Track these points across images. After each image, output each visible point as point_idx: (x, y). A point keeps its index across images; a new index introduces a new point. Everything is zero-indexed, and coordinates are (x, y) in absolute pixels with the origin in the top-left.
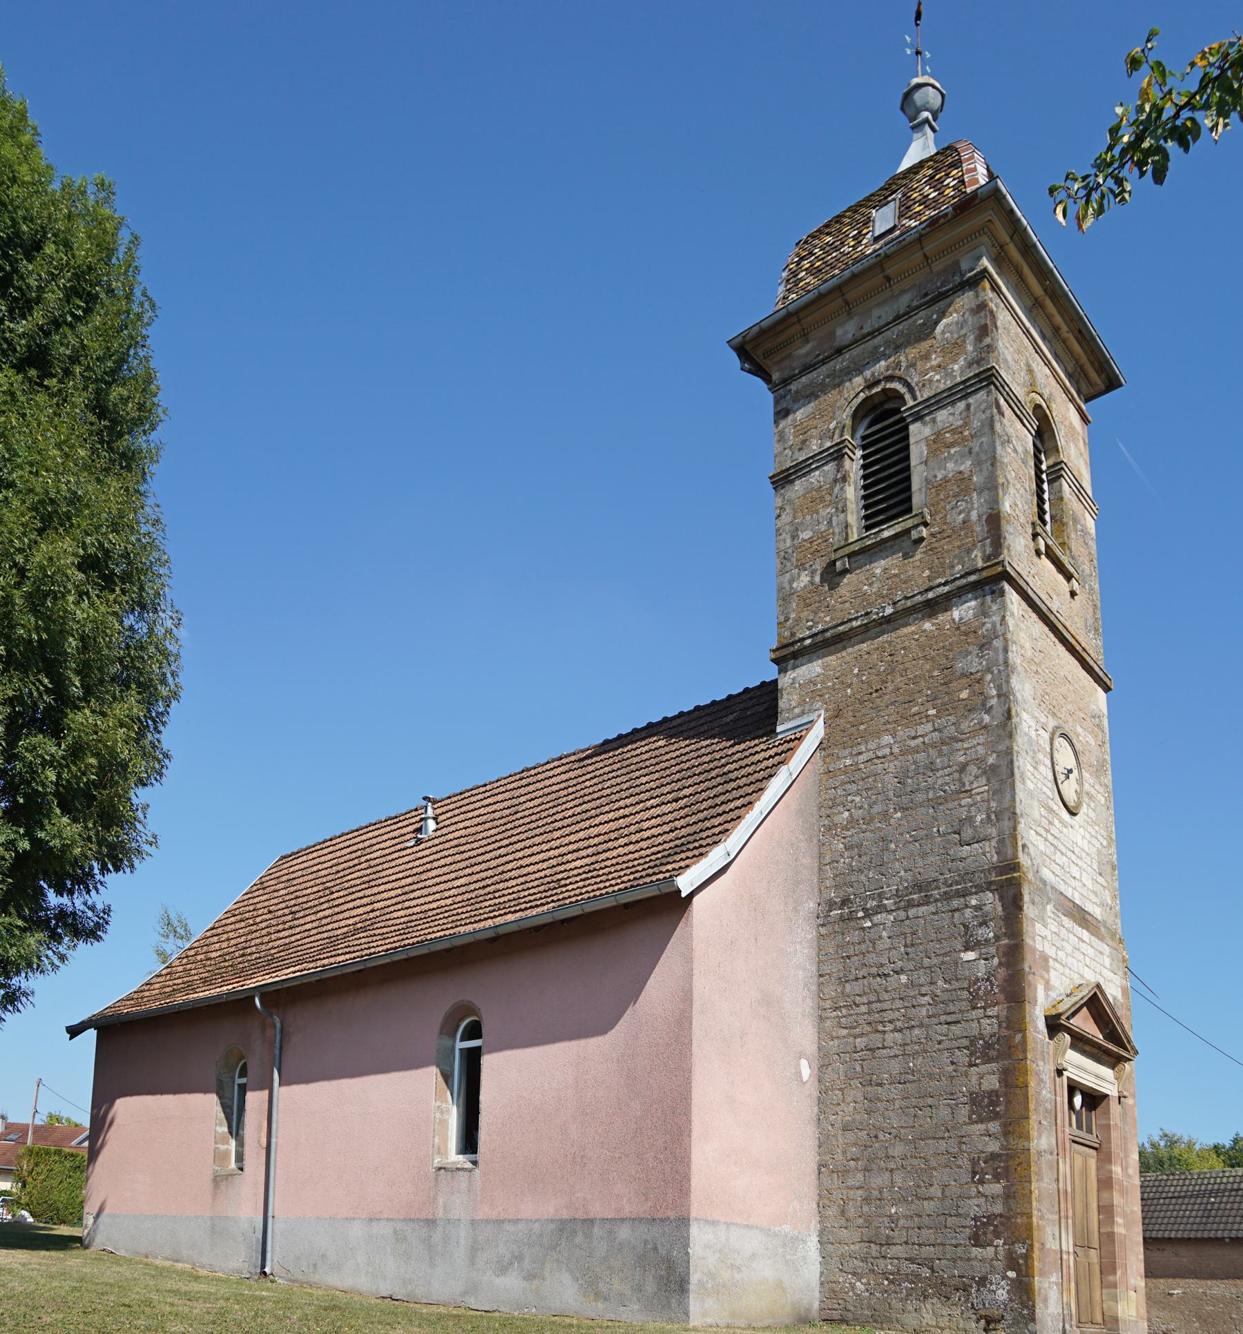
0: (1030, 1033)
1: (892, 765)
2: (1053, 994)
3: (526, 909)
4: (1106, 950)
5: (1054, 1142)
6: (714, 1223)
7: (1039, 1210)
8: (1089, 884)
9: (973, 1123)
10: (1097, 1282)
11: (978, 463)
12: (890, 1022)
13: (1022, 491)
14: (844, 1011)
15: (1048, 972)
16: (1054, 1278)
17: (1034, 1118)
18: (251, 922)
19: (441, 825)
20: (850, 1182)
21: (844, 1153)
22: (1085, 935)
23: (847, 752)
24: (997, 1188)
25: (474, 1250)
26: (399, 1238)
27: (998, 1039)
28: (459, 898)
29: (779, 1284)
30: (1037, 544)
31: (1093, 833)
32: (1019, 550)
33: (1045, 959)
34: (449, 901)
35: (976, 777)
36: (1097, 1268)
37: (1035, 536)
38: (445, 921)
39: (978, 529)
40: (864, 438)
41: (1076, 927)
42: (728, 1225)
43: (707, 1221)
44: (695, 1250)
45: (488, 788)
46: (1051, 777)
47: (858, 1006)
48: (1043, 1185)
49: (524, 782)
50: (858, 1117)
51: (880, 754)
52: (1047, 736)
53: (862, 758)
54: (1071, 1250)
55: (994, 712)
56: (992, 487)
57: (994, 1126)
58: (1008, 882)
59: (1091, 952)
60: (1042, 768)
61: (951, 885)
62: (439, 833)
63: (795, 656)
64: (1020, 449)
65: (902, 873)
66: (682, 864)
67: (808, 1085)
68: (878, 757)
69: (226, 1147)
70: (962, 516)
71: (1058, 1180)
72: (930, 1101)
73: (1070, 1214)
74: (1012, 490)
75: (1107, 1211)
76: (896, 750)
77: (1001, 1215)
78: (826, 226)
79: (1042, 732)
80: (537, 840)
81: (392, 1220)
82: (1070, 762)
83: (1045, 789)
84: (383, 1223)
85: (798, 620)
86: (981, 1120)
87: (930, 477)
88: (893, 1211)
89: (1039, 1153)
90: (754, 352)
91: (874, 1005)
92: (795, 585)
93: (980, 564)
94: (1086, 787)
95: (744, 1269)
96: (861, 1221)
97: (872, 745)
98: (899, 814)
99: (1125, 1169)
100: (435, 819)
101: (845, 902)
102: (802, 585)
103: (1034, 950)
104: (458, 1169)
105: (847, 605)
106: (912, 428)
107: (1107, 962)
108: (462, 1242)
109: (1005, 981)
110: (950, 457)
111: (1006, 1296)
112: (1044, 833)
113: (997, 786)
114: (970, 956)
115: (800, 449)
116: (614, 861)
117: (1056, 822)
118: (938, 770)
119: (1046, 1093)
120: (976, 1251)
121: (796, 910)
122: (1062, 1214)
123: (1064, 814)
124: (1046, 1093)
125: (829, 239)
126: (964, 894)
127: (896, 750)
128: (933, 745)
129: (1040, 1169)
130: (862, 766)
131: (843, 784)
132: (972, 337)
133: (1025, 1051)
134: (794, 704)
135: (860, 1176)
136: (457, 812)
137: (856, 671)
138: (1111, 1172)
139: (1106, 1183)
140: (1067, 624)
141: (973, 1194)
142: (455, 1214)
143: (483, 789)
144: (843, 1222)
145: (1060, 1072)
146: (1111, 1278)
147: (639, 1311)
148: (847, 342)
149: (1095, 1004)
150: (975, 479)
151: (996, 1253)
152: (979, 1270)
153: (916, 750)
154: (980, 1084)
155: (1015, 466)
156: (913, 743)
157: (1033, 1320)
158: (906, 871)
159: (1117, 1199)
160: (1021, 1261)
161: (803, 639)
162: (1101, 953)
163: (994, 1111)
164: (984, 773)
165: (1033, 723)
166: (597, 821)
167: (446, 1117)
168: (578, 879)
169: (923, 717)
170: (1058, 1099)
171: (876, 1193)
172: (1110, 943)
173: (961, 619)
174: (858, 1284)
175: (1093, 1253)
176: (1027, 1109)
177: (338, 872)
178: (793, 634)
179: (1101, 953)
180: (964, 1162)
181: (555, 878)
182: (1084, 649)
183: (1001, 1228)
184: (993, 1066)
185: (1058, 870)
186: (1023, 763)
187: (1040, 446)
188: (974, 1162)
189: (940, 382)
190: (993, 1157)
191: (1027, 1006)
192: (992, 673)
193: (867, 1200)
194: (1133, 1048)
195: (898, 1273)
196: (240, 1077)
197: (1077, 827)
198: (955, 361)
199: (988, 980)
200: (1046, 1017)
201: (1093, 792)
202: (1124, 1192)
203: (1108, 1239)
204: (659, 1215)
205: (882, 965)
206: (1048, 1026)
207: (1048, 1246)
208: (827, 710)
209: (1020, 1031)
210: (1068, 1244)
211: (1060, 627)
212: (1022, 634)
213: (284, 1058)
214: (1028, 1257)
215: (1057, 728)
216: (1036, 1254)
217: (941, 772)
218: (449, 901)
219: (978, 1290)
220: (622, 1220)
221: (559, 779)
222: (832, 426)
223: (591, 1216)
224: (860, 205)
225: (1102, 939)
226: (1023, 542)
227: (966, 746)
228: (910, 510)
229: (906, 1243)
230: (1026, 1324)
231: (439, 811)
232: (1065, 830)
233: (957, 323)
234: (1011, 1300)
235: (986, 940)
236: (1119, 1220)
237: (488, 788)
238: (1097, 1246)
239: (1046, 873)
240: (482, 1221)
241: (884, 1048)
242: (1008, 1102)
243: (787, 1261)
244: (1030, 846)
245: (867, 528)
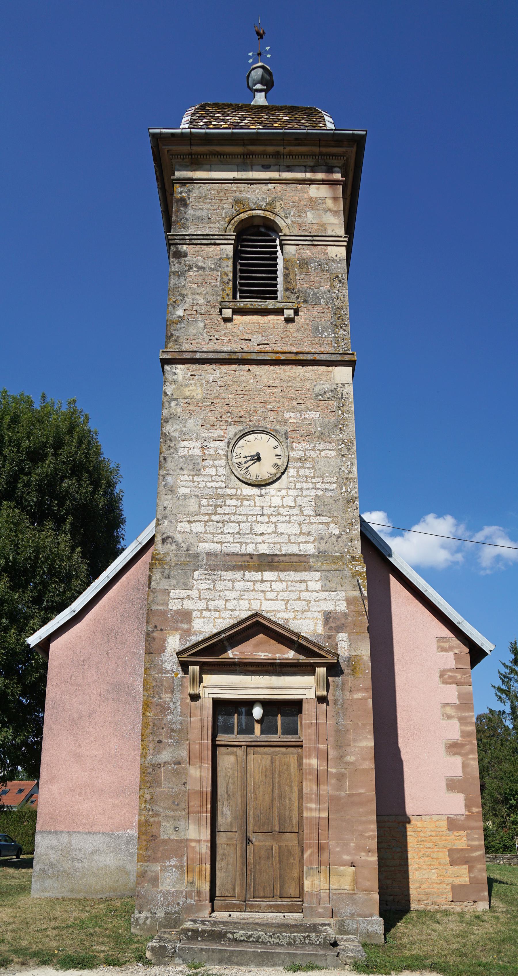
6: (56, 833)
182: (297, 353)
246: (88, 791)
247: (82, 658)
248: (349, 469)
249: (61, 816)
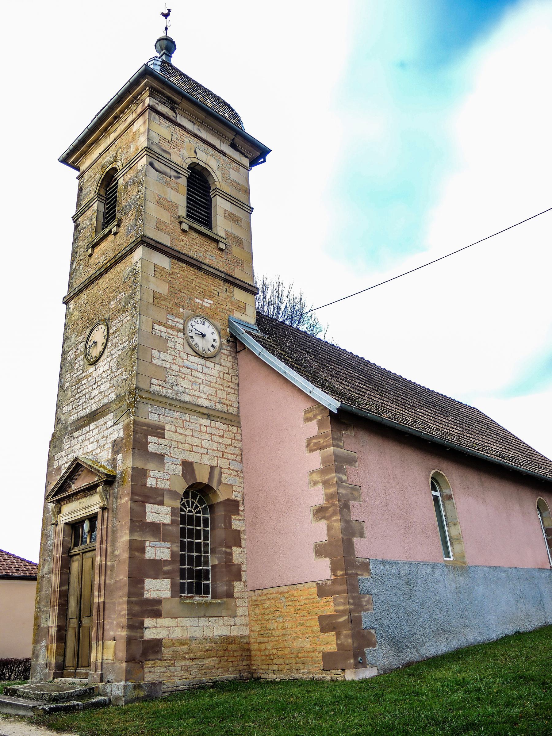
207: (42, 626)
211: (109, 264)
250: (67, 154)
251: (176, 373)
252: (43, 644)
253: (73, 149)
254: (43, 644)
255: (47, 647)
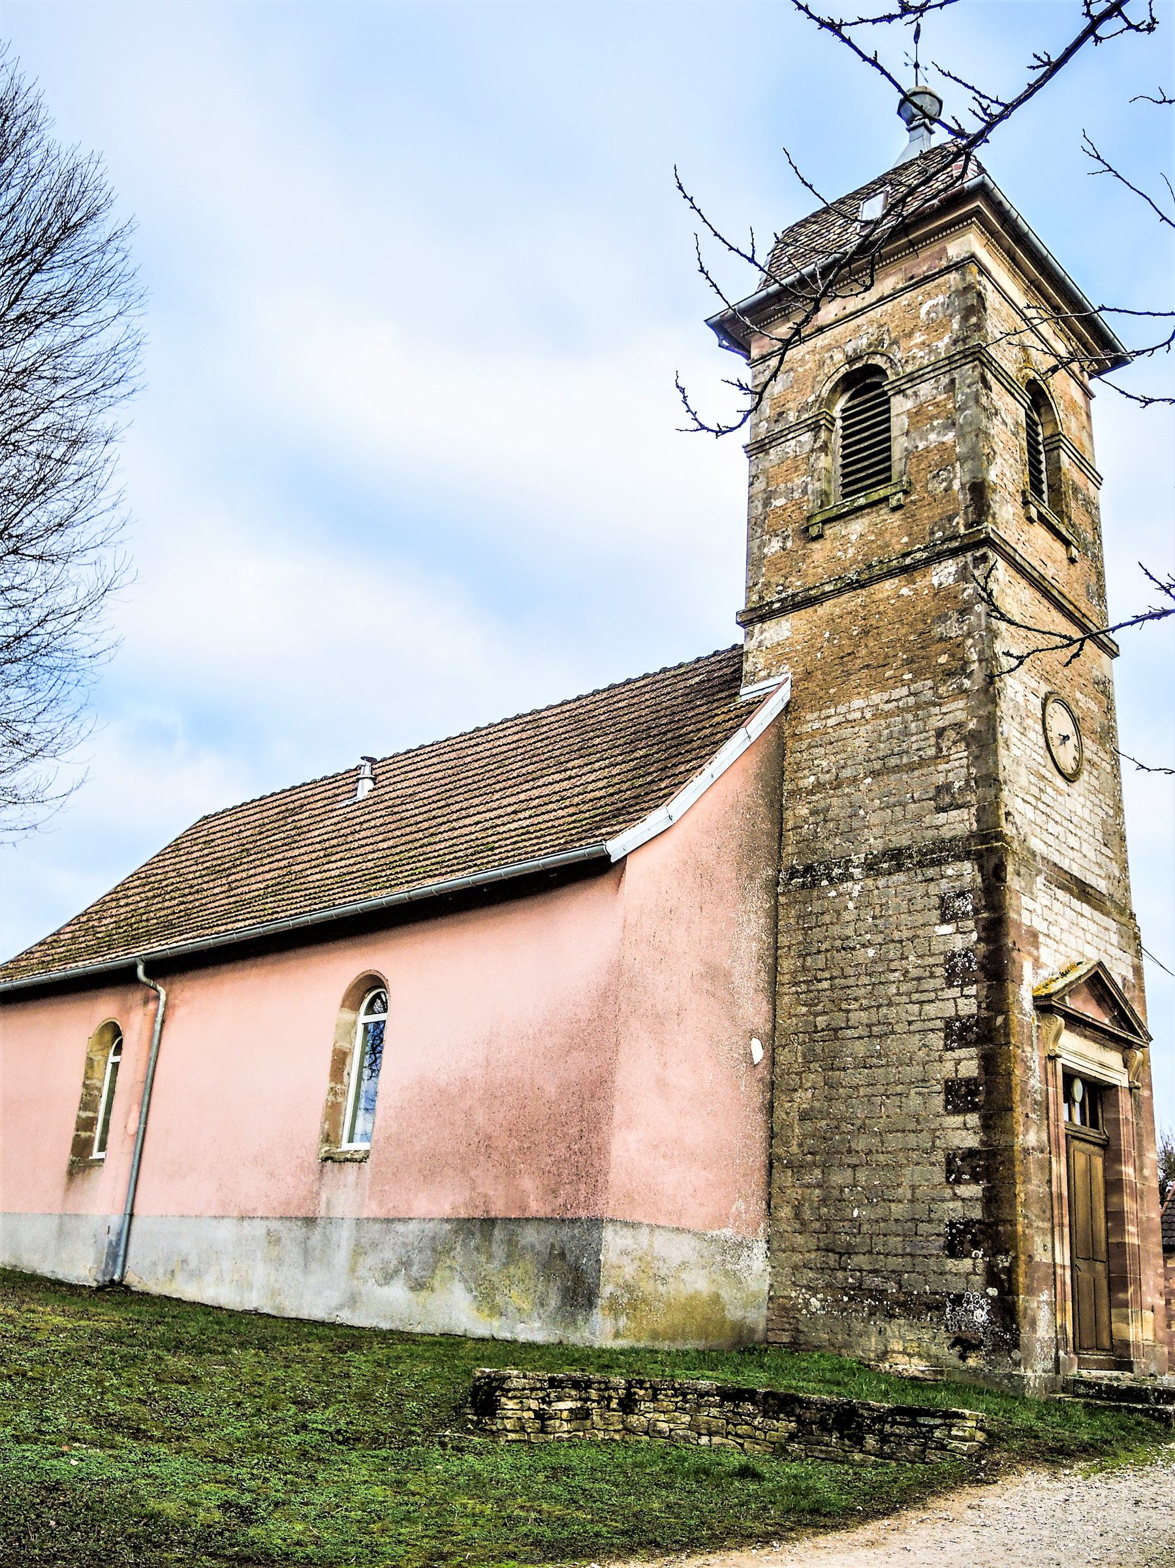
0: (1015, 1016)
1: (862, 728)
2: (1044, 973)
3: (447, 873)
4: (1113, 926)
5: (1045, 1138)
6: (633, 1225)
7: (1026, 1217)
8: (1091, 855)
9: (949, 1113)
10: (1104, 1301)
11: (961, 436)
12: (856, 999)
13: (1012, 461)
14: (804, 987)
15: (1037, 948)
16: (1045, 1296)
17: (1019, 1110)
18: (156, 885)
19: (379, 785)
20: (807, 1179)
21: (800, 1145)
22: (1086, 909)
23: (816, 715)
24: (973, 1190)
25: (358, 1251)
26: (273, 1239)
27: (977, 1021)
28: (382, 861)
29: (716, 1299)
30: (1027, 511)
31: (1097, 801)
32: (1007, 517)
33: (1034, 935)
34: (370, 864)
35: (955, 743)
36: (1104, 1283)
37: (1026, 503)
38: (360, 885)
39: (961, 497)
40: (843, 411)
41: (1074, 901)
42: (652, 1228)
43: (626, 1224)
44: (609, 1256)
45: (434, 748)
46: (1042, 742)
47: (819, 981)
48: (1031, 1187)
49: (473, 742)
50: (817, 1104)
51: (850, 717)
52: (1038, 702)
53: (832, 722)
54: (1067, 1263)
55: (975, 676)
56: (978, 457)
57: (973, 1119)
58: (989, 851)
59: (1093, 928)
60: (1031, 734)
61: (926, 854)
62: (375, 793)
63: (762, 619)
64: (1009, 421)
65: (872, 840)
66: (616, 828)
67: (760, 1068)
68: (848, 721)
69: (88, 1134)
70: (945, 484)
71: (1050, 1181)
72: (899, 1089)
73: (1066, 1221)
74: (998, 460)
75: (1116, 1218)
76: (868, 716)
77: (979, 1221)
78: (813, 215)
79: (1031, 697)
80: (476, 801)
81: (267, 1218)
82: (1069, 729)
83: (1035, 756)
84: (257, 1222)
85: (767, 585)
86: (957, 1111)
87: (910, 448)
88: (856, 1213)
89: (1026, 1151)
90: (734, 330)
91: (837, 981)
92: (765, 550)
93: (962, 531)
94: (1087, 754)
95: (671, 1280)
96: (817, 1225)
97: (842, 709)
98: (869, 780)
99: (1139, 1170)
100: (374, 779)
101: (809, 869)
102: (773, 550)
103: (1019, 925)
104: (348, 1160)
105: (820, 570)
106: (893, 400)
107: (1115, 939)
108: (344, 1244)
109: (985, 957)
110: (933, 429)
111: (985, 1317)
112: (1033, 802)
113: (977, 752)
114: (948, 929)
115: (776, 421)
116: (550, 824)
117: (1049, 790)
118: (913, 735)
119: (1035, 1083)
120: (951, 1264)
121: (751, 878)
122: (1056, 1221)
123: (1060, 782)
124: (1035, 1083)
125: (814, 227)
126: (939, 863)
127: (868, 716)
128: (907, 710)
129: (1027, 1169)
130: (830, 730)
131: (810, 747)
132: (958, 317)
133: (1007, 1035)
134: (760, 667)
135: (817, 1172)
136: (398, 772)
137: (827, 635)
138: (1121, 1172)
139: (1114, 1185)
140: (1065, 591)
141: (947, 1196)
142: (337, 1213)
143: (430, 749)
144: (798, 1226)
145: (1053, 1058)
146: (1121, 1296)
147: (540, 1329)
148: (828, 322)
149: (1098, 983)
150: (958, 449)
151: (974, 1265)
152: (957, 1286)
153: (888, 715)
154: (957, 1071)
155: (1003, 437)
156: (887, 707)
157: (1016, 1346)
158: (875, 839)
159: (1129, 1204)
160: (1003, 1276)
161: (772, 603)
162: (1106, 929)
163: (972, 1102)
164: (964, 739)
165: (1020, 688)
166: (540, 782)
167: (340, 1099)
168: (508, 842)
169: (899, 681)
170: (1051, 1089)
171: (836, 1193)
172: (1117, 917)
173: (940, 584)
174: (813, 1300)
175: (1100, 1267)
176: (1011, 1100)
177: (261, 833)
178: (761, 598)
179: (1106, 929)
180: (940, 1157)
181: (485, 841)
182: (1084, 615)
183: (980, 1237)
184: (973, 1051)
185: (1050, 840)
186: (1008, 728)
187: (1036, 417)
188: (950, 1161)
189: (923, 358)
190: (971, 1153)
191: (1010, 986)
192: (973, 637)
193: (824, 1201)
194: (1146, 1033)
195: (860, 1288)
196: (115, 1054)
197: (1076, 795)
198: (941, 339)
199: (965, 955)
200: (1035, 998)
201: (1096, 759)
202: (1138, 1195)
203: (1117, 1251)
204: (569, 1215)
205: (848, 938)
206: (1037, 1008)
207: (1037, 1259)
208: (794, 674)
209: (1003, 1013)
210: (1063, 1256)
211: (1055, 593)
212: (1008, 600)
213: (165, 1033)
214: (1010, 1271)
215: (1051, 693)
216: (1022, 1268)
217: (914, 738)
218: (370, 864)
219: (953, 1310)
220: (527, 1220)
221: (509, 739)
222: (810, 400)
223: (493, 1214)
224: (851, 196)
225: (1107, 914)
226: (1011, 510)
227: (944, 710)
228: (889, 479)
229: (870, 1252)
230: (1009, 1351)
231: (379, 771)
232: (1060, 798)
233: (943, 304)
234: (991, 1322)
235: (963, 913)
236: (1131, 1229)
237: (434, 748)
238: (1103, 1257)
239: (1035, 844)
240: (368, 1219)
241: (848, 1028)
242: (989, 1093)
243: (727, 1272)
244: (1015, 814)
245: (845, 496)
246: (676, 1153)
247: (668, 905)
248: (828, 678)
249: (639, 1193)
250: (1000, 203)
251: (94, 331)
252: (1042, 1298)
253: (1010, 217)
254: (1042, 1298)
255: (1053, 1305)
